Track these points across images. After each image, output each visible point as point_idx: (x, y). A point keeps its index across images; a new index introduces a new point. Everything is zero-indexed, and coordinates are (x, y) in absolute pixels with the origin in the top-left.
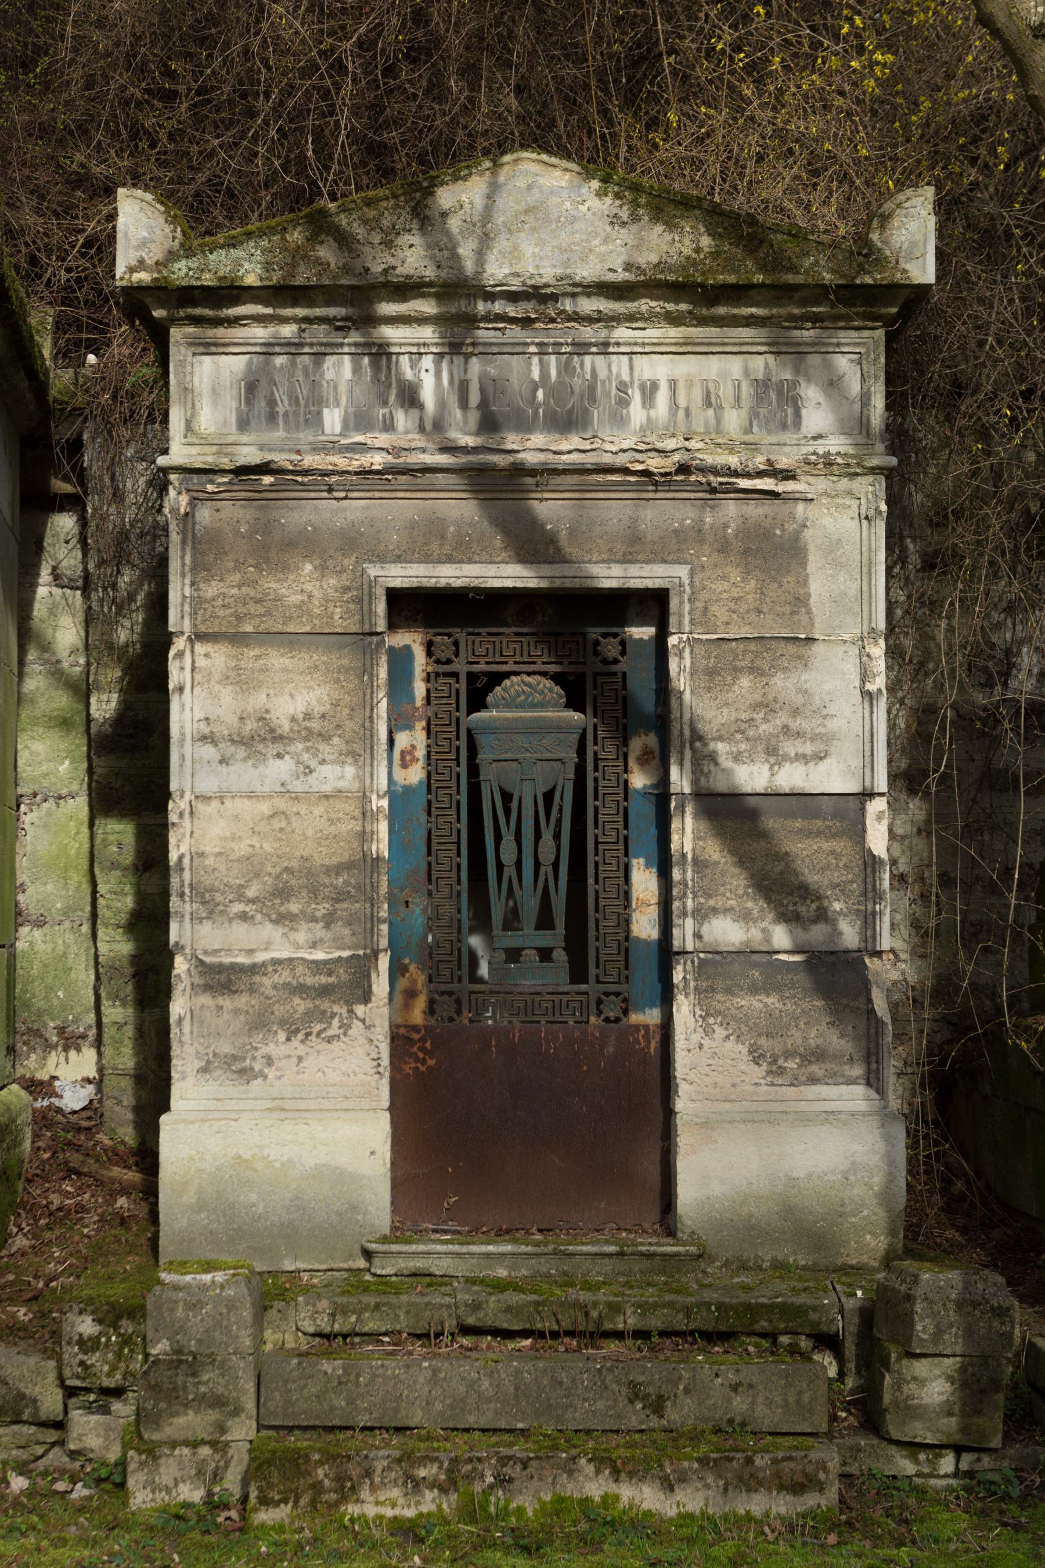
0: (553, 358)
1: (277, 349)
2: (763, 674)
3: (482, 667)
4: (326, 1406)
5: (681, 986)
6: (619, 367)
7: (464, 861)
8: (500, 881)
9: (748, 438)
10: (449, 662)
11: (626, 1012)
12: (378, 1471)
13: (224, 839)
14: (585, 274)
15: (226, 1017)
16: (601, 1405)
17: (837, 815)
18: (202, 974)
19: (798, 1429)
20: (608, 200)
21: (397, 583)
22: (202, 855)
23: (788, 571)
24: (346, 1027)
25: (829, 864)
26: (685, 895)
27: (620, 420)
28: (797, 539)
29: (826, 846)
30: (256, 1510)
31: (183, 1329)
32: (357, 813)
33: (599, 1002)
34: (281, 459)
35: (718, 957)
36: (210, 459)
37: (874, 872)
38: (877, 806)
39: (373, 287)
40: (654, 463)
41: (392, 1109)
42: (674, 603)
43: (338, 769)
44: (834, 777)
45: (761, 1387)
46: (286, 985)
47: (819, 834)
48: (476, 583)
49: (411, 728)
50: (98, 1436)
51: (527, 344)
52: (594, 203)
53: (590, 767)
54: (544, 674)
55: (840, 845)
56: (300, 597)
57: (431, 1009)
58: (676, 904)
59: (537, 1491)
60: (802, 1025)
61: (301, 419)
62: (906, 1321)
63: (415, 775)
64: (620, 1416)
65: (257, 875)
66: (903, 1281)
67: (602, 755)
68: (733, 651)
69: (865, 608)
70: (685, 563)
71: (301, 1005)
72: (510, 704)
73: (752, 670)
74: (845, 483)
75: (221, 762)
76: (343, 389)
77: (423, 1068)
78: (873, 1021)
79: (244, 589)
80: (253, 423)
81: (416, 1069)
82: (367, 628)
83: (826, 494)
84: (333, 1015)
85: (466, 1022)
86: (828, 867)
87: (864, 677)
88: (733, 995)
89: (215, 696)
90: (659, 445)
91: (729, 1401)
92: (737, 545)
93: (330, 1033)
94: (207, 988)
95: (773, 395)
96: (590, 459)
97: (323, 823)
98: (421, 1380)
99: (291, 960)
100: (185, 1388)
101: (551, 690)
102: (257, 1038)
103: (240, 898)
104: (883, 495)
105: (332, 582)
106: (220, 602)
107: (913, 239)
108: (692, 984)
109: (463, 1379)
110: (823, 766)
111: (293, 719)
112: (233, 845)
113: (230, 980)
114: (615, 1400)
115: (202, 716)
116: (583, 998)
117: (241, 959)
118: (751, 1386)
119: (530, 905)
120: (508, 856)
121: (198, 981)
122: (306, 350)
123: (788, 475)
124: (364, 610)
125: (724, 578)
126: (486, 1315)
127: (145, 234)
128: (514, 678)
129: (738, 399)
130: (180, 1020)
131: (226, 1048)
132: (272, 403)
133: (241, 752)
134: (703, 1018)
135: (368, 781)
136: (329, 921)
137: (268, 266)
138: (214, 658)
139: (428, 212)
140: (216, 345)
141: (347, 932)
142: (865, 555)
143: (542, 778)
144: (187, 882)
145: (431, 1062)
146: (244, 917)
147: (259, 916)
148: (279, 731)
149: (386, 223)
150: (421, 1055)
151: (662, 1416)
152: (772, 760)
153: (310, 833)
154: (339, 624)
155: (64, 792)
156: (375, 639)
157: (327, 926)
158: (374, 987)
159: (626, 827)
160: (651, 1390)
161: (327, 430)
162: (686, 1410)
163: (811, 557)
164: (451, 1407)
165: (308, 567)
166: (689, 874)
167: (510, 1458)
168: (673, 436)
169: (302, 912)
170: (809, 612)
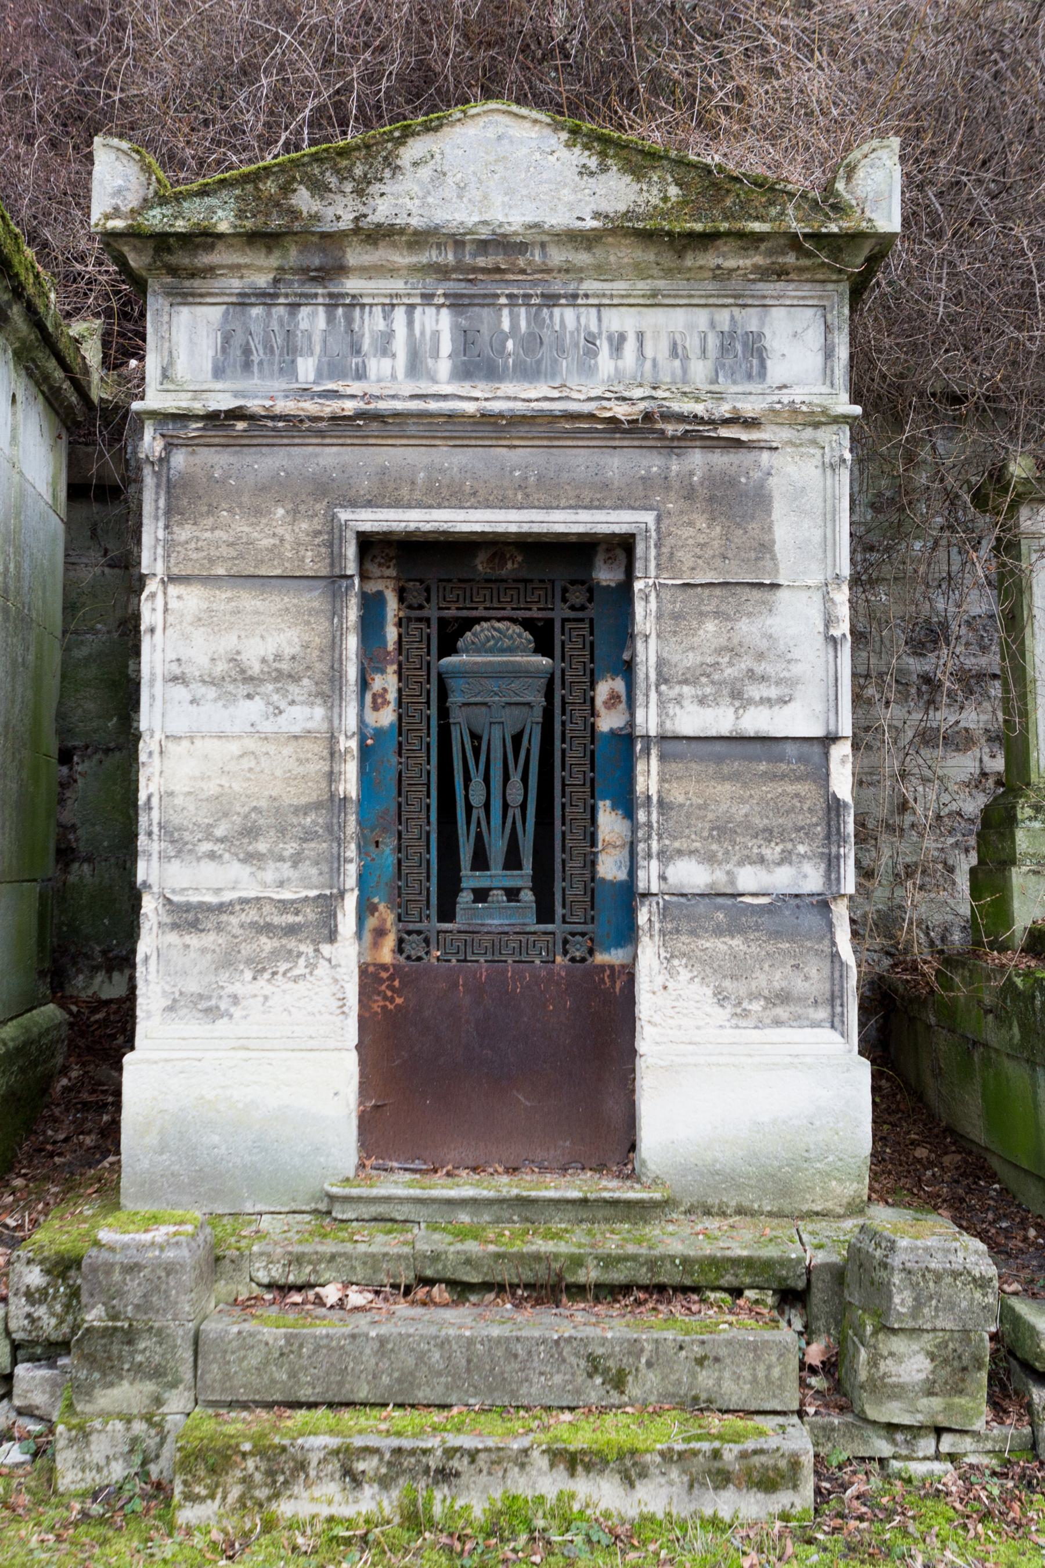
0: (523, 310)
1: (253, 300)
2: (728, 618)
3: (452, 613)
4: (266, 1377)
5: (647, 927)
6: (588, 319)
7: (434, 802)
8: (468, 823)
9: (715, 388)
10: (421, 607)
11: (591, 952)
12: (314, 1463)
13: (194, 778)
14: (554, 222)
15: (193, 955)
16: (558, 1379)
17: (801, 759)
18: (170, 912)
19: (768, 1407)
20: (577, 150)
21: (367, 527)
22: (171, 794)
23: (753, 518)
24: (312, 967)
25: (793, 808)
26: (649, 837)
27: (587, 369)
28: (762, 486)
29: (791, 789)
30: (180, 1506)
31: (120, 1294)
32: (326, 753)
33: (565, 942)
34: (254, 405)
35: (683, 900)
36: (184, 404)
37: (838, 815)
38: (842, 751)
39: (343, 234)
40: (621, 411)
41: (358, 1047)
42: (640, 549)
43: (307, 710)
44: (798, 720)
45: (728, 1361)
46: (253, 925)
47: (783, 777)
48: (445, 527)
49: (383, 671)
50: (44, 1392)
51: (497, 296)
52: (564, 153)
53: (558, 711)
54: (513, 620)
55: (803, 788)
56: (272, 541)
57: (400, 949)
58: (641, 847)
59: (485, 1489)
60: (766, 967)
61: (276, 367)
62: (883, 1290)
63: (387, 717)
64: (578, 1392)
65: (226, 815)
66: (878, 1245)
67: (569, 699)
68: (698, 595)
69: (829, 554)
70: (652, 509)
71: (267, 944)
72: (480, 649)
73: (717, 614)
74: (809, 433)
75: (192, 702)
76: (317, 338)
77: (391, 1007)
78: (837, 965)
79: (217, 533)
80: (228, 371)
81: (384, 1007)
82: (337, 571)
83: (791, 443)
84: (300, 954)
85: (434, 961)
86: (792, 809)
87: (828, 623)
88: (698, 937)
89: (186, 637)
90: (626, 394)
91: (694, 1375)
92: (703, 492)
93: (296, 972)
94: (175, 926)
95: (739, 347)
96: (558, 406)
97: (292, 764)
98: (368, 1351)
99: (258, 899)
100: (120, 1357)
101: (520, 636)
102: (224, 976)
103: (209, 836)
104: (847, 443)
105: (304, 526)
106: (193, 545)
107: (878, 191)
108: (657, 926)
109: (413, 1350)
110: (788, 709)
111: (264, 661)
112: (204, 785)
113: (197, 919)
114: (573, 1374)
115: (174, 657)
116: (549, 938)
117: (210, 899)
118: (717, 1360)
119: (497, 847)
120: (477, 798)
121: (167, 919)
122: (282, 300)
123: (751, 423)
124: (336, 558)
125: (691, 524)
126: (445, 1267)
127: (120, 182)
128: (485, 625)
129: (704, 351)
130: (147, 958)
131: (193, 987)
132: (247, 351)
133: (212, 692)
134: (668, 960)
135: (336, 722)
136: (296, 860)
137: (241, 214)
138: (189, 600)
139: (399, 162)
140: (193, 295)
141: (314, 871)
142: (829, 502)
143: (512, 720)
144: (155, 821)
145: (399, 1001)
146: (212, 856)
147: (227, 856)
148: (250, 673)
149: (358, 171)
150: (389, 993)
151: (622, 1393)
152: (737, 704)
153: (278, 773)
154: (310, 567)
155: (112, 745)
156: (345, 583)
157: (295, 865)
158: (340, 928)
159: (592, 770)
160: (611, 1363)
161: (301, 378)
162: (648, 1384)
163: (776, 505)
164: (399, 1381)
165: (281, 511)
166: (654, 817)
167: (456, 1450)
168: (641, 385)
169: (270, 851)
170: (774, 558)
